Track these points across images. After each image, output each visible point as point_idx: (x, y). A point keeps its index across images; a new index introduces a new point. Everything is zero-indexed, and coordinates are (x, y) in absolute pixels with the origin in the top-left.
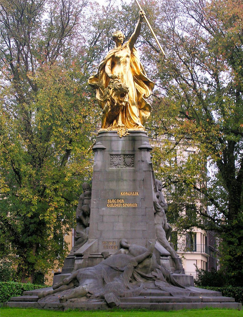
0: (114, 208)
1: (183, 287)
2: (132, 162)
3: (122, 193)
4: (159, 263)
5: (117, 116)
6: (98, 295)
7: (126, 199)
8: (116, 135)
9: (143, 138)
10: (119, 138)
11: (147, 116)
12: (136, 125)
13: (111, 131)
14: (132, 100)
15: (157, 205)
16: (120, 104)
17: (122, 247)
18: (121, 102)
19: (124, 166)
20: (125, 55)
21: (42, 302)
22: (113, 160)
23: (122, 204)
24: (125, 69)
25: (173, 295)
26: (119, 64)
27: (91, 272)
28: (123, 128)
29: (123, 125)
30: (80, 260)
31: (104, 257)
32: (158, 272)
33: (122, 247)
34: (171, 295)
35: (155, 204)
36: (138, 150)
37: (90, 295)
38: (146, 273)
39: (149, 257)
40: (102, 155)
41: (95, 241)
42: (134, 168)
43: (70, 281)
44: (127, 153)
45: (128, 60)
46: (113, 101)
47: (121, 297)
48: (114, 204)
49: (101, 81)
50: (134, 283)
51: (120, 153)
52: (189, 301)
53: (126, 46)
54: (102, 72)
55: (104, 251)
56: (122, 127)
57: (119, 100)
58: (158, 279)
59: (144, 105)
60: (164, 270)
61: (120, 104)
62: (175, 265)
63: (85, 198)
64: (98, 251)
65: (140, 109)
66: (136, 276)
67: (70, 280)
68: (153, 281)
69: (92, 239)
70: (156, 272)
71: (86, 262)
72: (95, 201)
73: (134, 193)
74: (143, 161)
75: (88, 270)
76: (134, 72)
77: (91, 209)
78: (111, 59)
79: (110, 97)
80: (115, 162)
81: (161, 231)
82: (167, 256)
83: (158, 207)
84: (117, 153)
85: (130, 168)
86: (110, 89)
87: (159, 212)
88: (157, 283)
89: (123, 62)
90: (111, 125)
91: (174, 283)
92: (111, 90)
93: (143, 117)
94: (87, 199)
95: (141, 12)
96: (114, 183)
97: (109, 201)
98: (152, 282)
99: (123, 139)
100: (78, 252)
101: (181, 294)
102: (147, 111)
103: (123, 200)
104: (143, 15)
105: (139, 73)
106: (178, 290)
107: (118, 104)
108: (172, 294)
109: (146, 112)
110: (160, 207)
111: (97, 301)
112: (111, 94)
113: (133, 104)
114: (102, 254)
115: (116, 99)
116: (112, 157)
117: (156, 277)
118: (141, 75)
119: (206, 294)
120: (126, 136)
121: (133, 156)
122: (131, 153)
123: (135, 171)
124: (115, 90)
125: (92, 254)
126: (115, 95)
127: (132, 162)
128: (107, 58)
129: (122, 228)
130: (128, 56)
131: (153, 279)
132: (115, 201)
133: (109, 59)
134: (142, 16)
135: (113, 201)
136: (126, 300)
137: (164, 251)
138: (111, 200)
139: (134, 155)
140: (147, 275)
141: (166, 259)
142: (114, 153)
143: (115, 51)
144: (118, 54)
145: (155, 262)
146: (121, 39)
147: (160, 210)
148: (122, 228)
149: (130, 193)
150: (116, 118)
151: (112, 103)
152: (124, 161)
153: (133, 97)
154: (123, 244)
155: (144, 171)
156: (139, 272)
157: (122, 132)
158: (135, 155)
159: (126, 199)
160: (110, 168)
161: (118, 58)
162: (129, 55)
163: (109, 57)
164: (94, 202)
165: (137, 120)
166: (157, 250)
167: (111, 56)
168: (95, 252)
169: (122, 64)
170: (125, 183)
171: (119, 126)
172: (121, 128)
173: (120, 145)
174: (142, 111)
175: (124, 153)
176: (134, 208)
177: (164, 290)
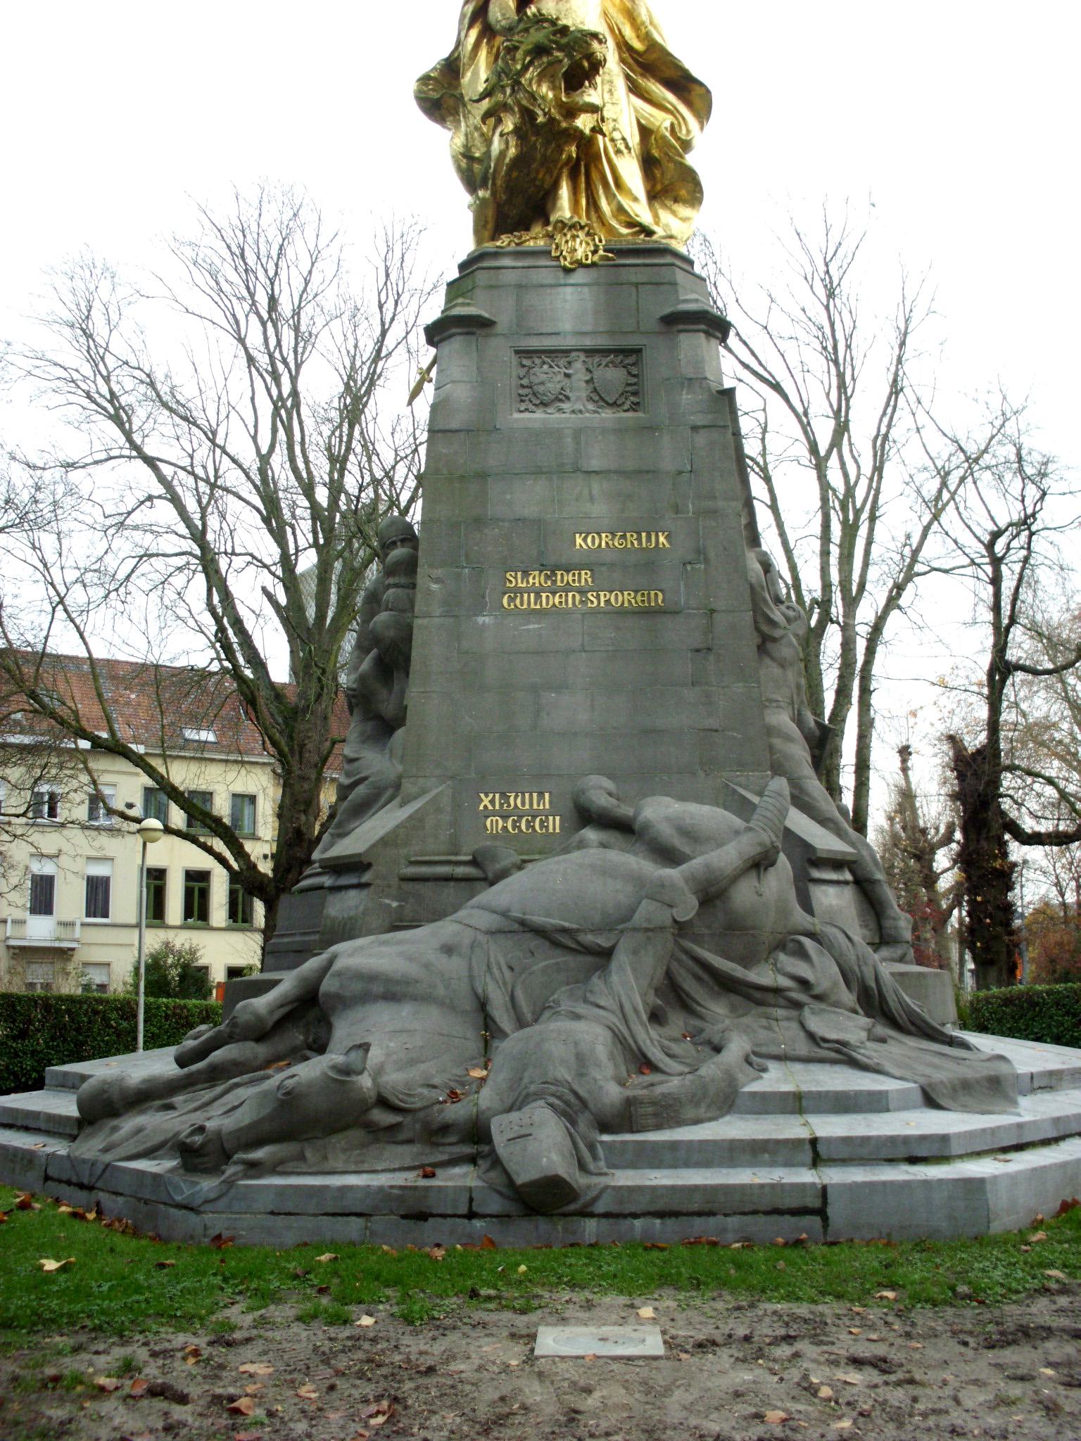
2: (629, 389)
3: (579, 541)
10: (561, 274)
15: (765, 600)
19: (591, 406)
22: (535, 380)
23: (582, 592)
25: (942, 1102)
38: (747, 961)
40: (475, 354)
41: (441, 788)
43: (278, 1015)
44: (602, 342)
48: (538, 596)
50: (677, 1022)
51: (569, 342)
58: (819, 998)
63: (391, 580)
67: (282, 1006)
68: (794, 1013)
70: (802, 954)
72: (437, 581)
73: (644, 535)
77: (415, 632)
80: (541, 389)
82: (837, 864)
83: (769, 612)
84: (548, 343)
85: (617, 415)
88: (817, 1024)
91: (902, 1019)
94: (396, 586)
96: (540, 488)
97: (515, 580)
98: (788, 1019)
99: (580, 276)
114: (474, 862)
116: (525, 362)
117: (804, 984)
120: (594, 265)
121: (628, 355)
125: (419, 858)
127: (629, 389)
132: (547, 577)
135: (536, 579)
141: (838, 883)
142: (534, 343)
147: (777, 633)
149: (624, 537)
151: (522, 117)
152: (587, 382)
154: (594, 798)
158: (647, 354)
160: (516, 415)
164: (435, 587)
174: (665, 206)
175: (588, 342)
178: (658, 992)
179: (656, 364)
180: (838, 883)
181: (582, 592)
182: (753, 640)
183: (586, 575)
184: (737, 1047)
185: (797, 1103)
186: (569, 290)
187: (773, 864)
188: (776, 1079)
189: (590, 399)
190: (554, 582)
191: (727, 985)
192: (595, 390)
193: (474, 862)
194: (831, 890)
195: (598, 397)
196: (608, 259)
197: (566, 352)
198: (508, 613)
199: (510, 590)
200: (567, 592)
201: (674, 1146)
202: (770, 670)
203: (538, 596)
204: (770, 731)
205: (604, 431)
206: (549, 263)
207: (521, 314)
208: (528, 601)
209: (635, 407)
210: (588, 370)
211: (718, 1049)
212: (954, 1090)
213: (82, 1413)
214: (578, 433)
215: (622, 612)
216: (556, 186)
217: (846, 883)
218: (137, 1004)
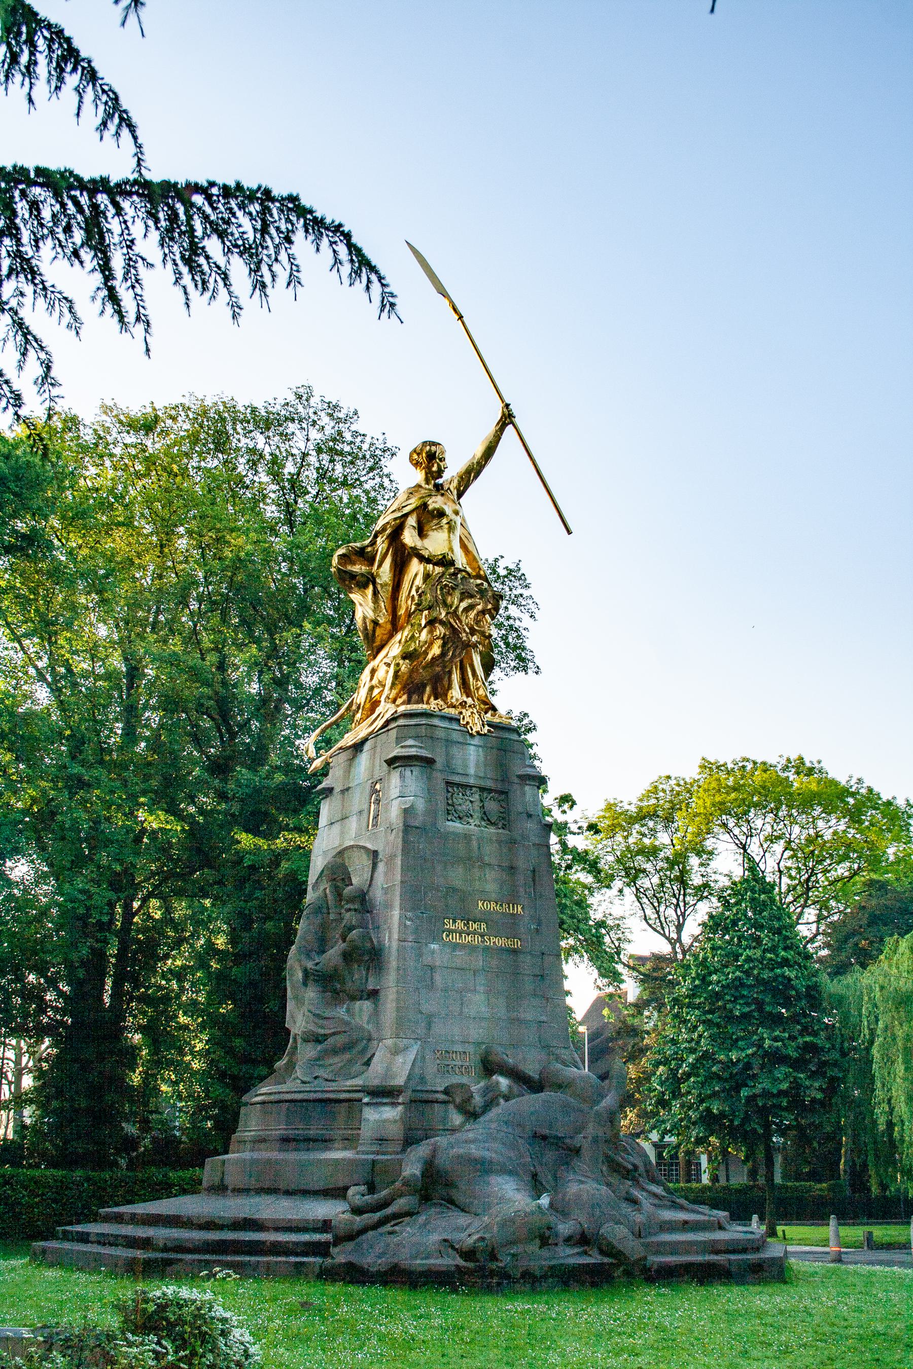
0: (463, 946)
3: (480, 904)
23: (482, 936)
30: (387, 1108)
31: (454, 1102)
36: (516, 780)
44: (489, 784)
48: (461, 936)
51: (472, 781)
97: (450, 925)
103: (483, 926)
122: (499, 787)
132: (465, 925)
135: (460, 925)
138: (454, 922)
142: (457, 779)
149: (501, 905)
175: (482, 783)
176: (515, 952)
186: (472, 748)
189: (482, 819)
190: (468, 928)
192: (485, 813)
195: (486, 817)
200: (475, 934)
201: (664, 1244)
203: (461, 936)
206: (459, 728)
207: (449, 758)
210: (481, 801)
213: (504, 1360)
214: (480, 839)
215: (501, 950)
218: (254, 1162)
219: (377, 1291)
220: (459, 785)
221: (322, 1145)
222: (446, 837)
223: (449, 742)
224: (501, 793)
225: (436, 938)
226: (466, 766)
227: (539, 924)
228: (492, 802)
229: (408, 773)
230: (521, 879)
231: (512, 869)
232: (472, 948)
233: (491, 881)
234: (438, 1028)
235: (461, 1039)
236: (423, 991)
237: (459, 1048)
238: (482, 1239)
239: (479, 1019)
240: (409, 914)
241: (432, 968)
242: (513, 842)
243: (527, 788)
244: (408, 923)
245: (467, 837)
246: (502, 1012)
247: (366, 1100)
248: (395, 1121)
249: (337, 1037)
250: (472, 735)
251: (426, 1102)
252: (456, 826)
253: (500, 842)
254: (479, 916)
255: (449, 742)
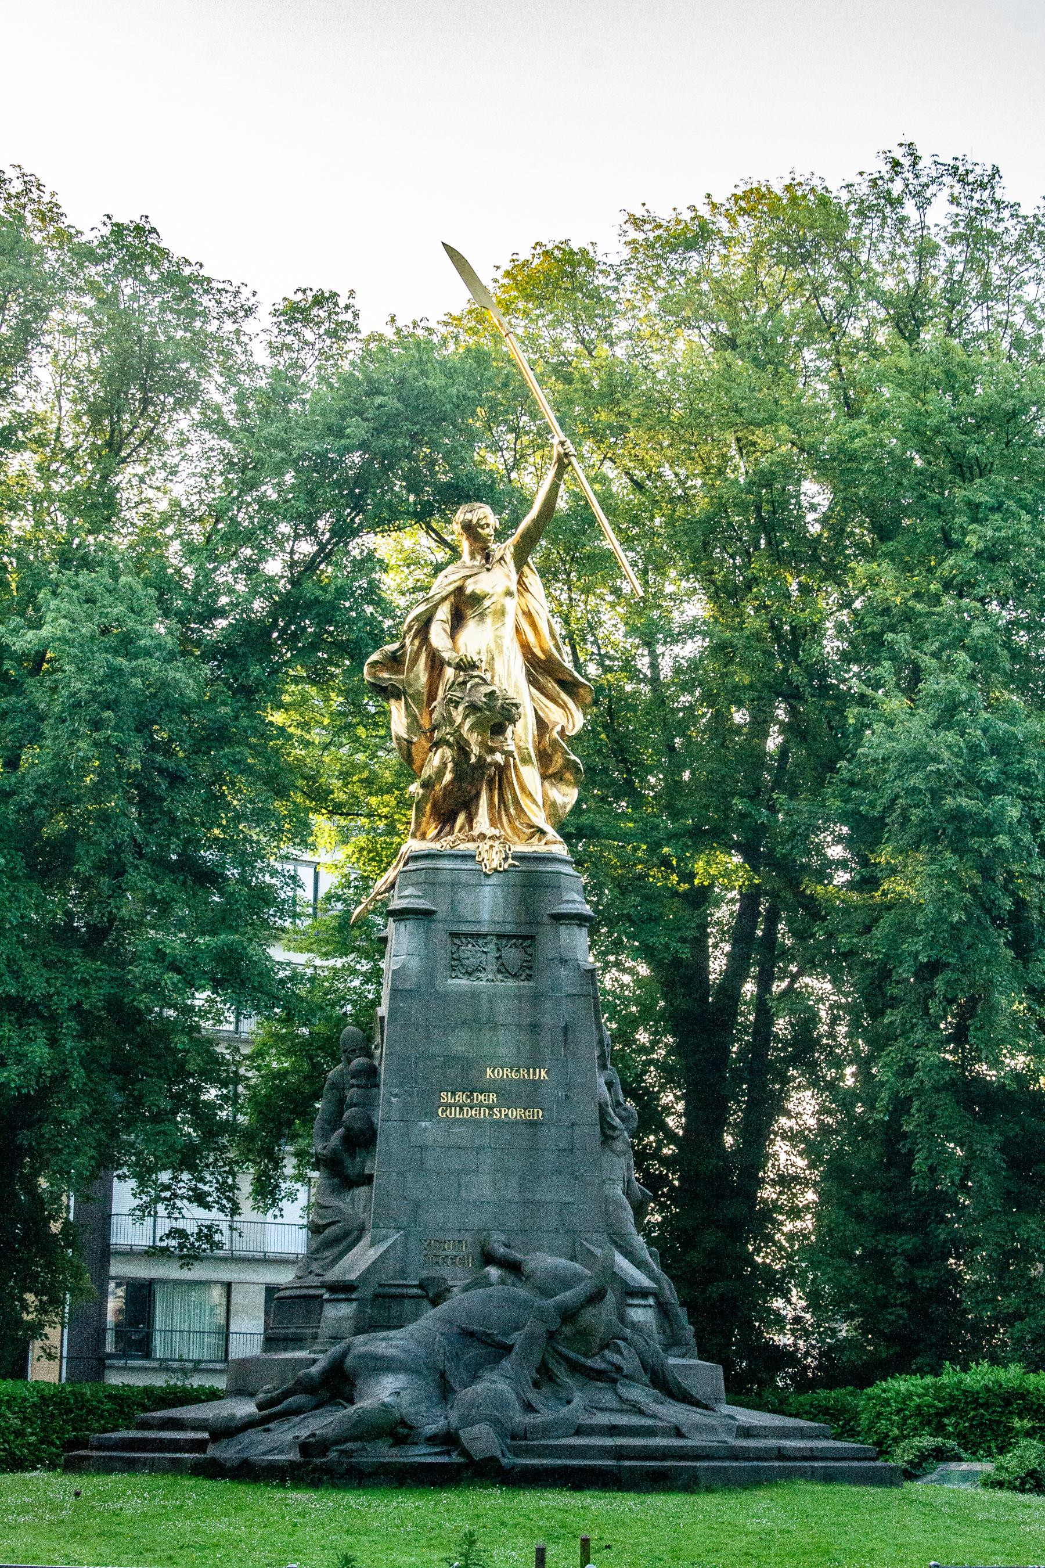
0: (464, 1122)
1: (706, 1407)
3: (489, 1072)
4: (622, 1318)
5: (471, 800)
6: (430, 1429)
7: (506, 1094)
8: (469, 865)
9: (564, 881)
11: (566, 800)
12: (537, 836)
13: (453, 852)
14: (521, 744)
16: (489, 759)
17: (488, 1258)
18: (492, 751)
19: (500, 977)
20: (500, 589)
21: (226, 1452)
23: (490, 1108)
24: (498, 638)
26: (482, 616)
27: (397, 1347)
28: (496, 844)
29: (496, 832)
30: (343, 1305)
31: (427, 1297)
32: (625, 1352)
33: (488, 1258)
34: (678, 1433)
35: (602, 1107)
36: (548, 920)
37: (406, 1431)
39: (596, 1297)
42: (531, 984)
44: (509, 929)
45: (511, 605)
46: (462, 749)
47: (514, 1437)
48: (461, 1109)
49: (412, 675)
51: (484, 929)
52: (734, 1454)
53: (502, 558)
54: (417, 642)
55: (425, 1273)
56: (491, 838)
57: (483, 745)
58: (626, 1377)
59: (558, 761)
60: (642, 1343)
61: (489, 759)
62: (667, 1325)
64: (403, 1273)
65: (544, 777)
66: (552, 1364)
69: (385, 1231)
70: (619, 1352)
71: (364, 1313)
72: (396, 1096)
74: (564, 961)
75: (384, 1339)
76: (526, 648)
78: (452, 598)
79: (452, 735)
81: (620, 1206)
82: (644, 1293)
86: (456, 707)
87: (614, 1138)
89: (495, 613)
90: (447, 828)
91: (674, 1390)
92: (461, 708)
93: (554, 804)
94: (358, 1086)
95: (562, 444)
96: (465, 1034)
97: (446, 1098)
99: (493, 881)
100: (333, 1275)
101: (711, 1430)
102: (568, 783)
103: (493, 1097)
104: (566, 455)
105: (543, 651)
106: (698, 1416)
107: (480, 758)
108: (684, 1430)
109: (564, 788)
110: (616, 1122)
111: (436, 1450)
112: (458, 720)
113: (526, 760)
114: (420, 1286)
115: (473, 739)
116: (456, 941)
117: (619, 1369)
118: (550, 658)
119: (785, 1433)
120: (505, 871)
122: (523, 931)
123: (537, 997)
124: (473, 708)
126: (471, 729)
128: (438, 597)
129: (489, 1193)
130: (509, 593)
131: (611, 1377)
133: (445, 599)
134: (566, 461)
135: (461, 1097)
136: (529, 1452)
137: (640, 1278)
138: (453, 1094)
139: (532, 938)
140: (589, 1362)
141: (645, 1306)
142: (464, 928)
143: (466, 572)
144: (475, 583)
145: (614, 1316)
146: (487, 531)
147: (616, 1133)
148: (489, 1193)
150: (469, 805)
153: (526, 734)
155: (568, 996)
156: (566, 1351)
157: (493, 858)
158: (539, 937)
159: (506, 1094)
161: (476, 599)
162: (514, 588)
163: (444, 593)
165: (539, 817)
166: (615, 1277)
167: (451, 588)
168: (394, 1279)
169: (489, 620)
170: (502, 1035)
171: (482, 836)
172: (490, 843)
173: (486, 900)
174: (552, 784)
175: (498, 929)
176: (533, 1124)
177: (651, 1416)
178: (538, 1371)
179: (546, 948)
180: (645, 1306)
181: (490, 1108)
182: (599, 1137)
183: (493, 1097)
184: (579, 1400)
185: (614, 1430)
186: (487, 889)
187: (604, 1297)
188: (603, 1419)
189: (499, 971)
191: (575, 1368)
193: (420, 1286)
194: (640, 1311)
195: (503, 969)
196: (514, 866)
197: (485, 936)
198: (440, 1121)
199: (444, 1105)
201: (547, 1447)
202: (607, 1158)
203: (461, 1109)
204: (606, 1200)
205: (508, 997)
207: (454, 905)
208: (454, 1113)
209: (529, 978)
210: (499, 950)
211: (569, 1402)
212: (528, 1278)
214: (492, 997)
215: (516, 1123)
216: (478, 795)
217: (650, 1306)
219: (223, 1485)
220: (466, 935)
221: (282, 1345)
222: (443, 998)
223: (456, 885)
224: (525, 938)
225: (430, 1114)
226: (477, 911)
227: (570, 1088)
228: (513, 950)
229: (402, 928)
230: (545, 1038)
231: (535, 1027)
232: (476, 1123)
233: (504, 1044)
234: (429, 1217)
235: (456, 1226)
236: (409, 1177)
237: (451, 1236)
238: (313, 1435)
239: (479, 1204)
240: (395, 1090)
241: (422, 1148)
242: (537, 997)
243: (562, 929)
244: (394, 1100)
245: (475, 995)
246: (513, 1194)
247: (326, 1296)
248: (348, 1318)
249: (332, 1227)
250: (487, 876)
251: (394, 1297)
252: (463, 983)
253: (519, 997)
254: (486, 1086)
255: (456, 885)
